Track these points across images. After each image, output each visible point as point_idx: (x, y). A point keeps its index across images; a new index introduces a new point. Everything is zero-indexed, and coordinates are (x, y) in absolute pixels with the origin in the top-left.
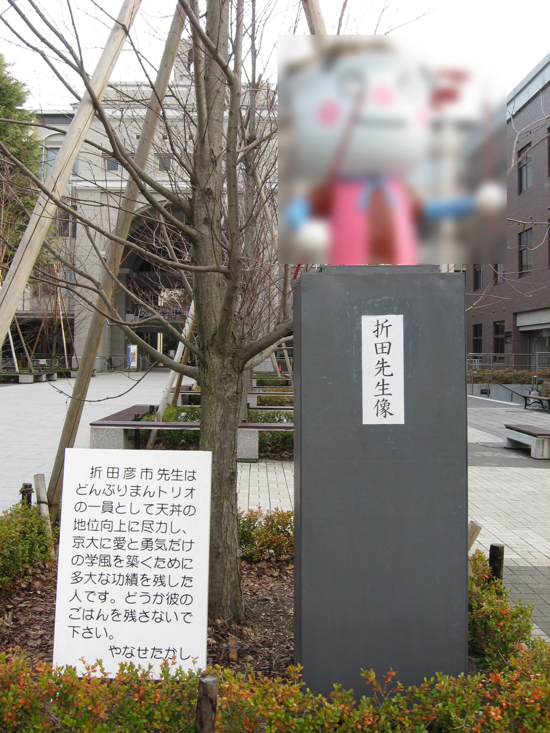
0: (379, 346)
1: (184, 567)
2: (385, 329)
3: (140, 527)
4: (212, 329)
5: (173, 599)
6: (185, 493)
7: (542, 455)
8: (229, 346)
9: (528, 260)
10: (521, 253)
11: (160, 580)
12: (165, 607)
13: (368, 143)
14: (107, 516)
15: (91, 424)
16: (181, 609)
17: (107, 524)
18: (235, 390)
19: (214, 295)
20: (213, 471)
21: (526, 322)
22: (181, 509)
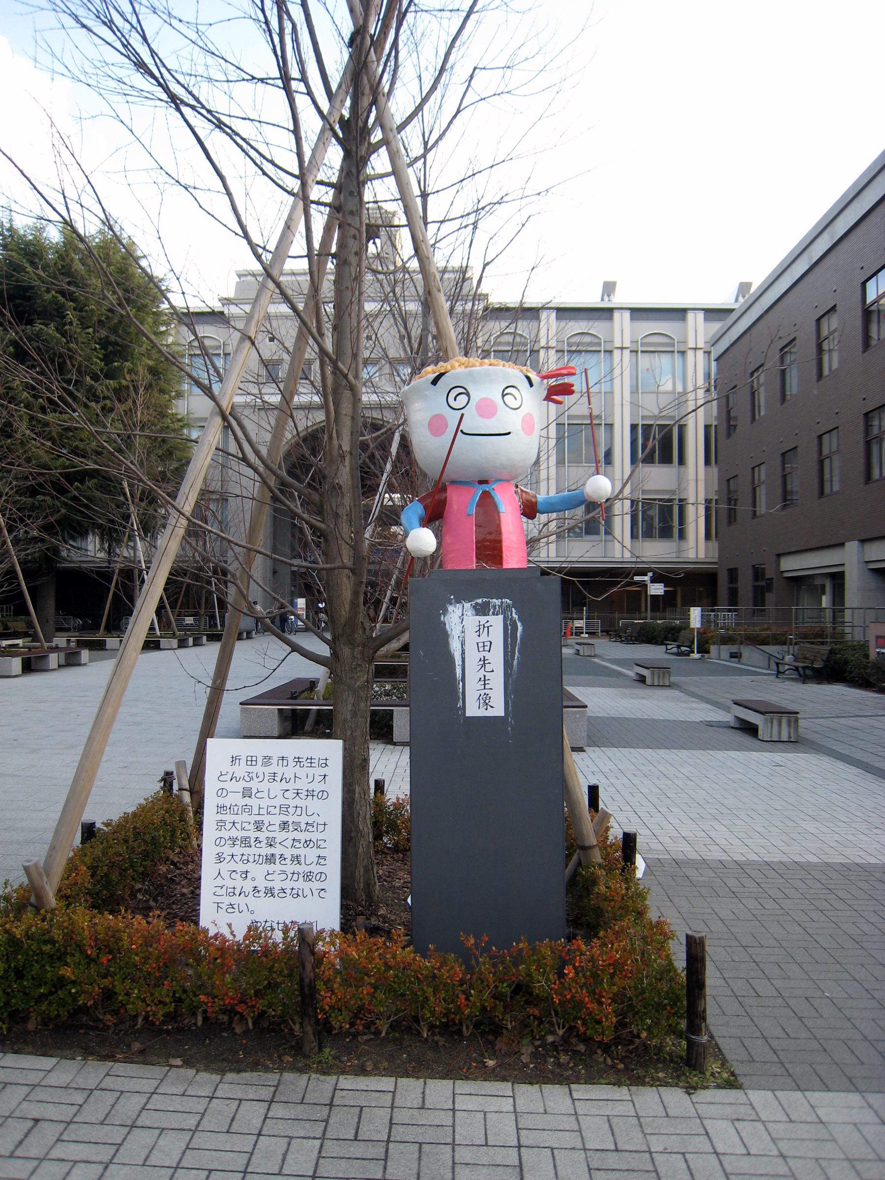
0: (481, 645)
1: (318, 847)
2: (486, 629)
3: (277, 811)
4: (343, 620)
5: (308, 877)
6: (318, 779)
7: (771, 737)
8: (359, 636)
9: (794, 484)
10: (784, 478)
11: (296, 859)
12: (301, 884)
13: (471, 453)
14: (247, 800)
15: (241, 704)
16: (316, 885)
17: (247, 809)
18: (365, 679)
19: (344, 588)
20: (344, 757)
21: (792, 565)
22: (315, 793)
